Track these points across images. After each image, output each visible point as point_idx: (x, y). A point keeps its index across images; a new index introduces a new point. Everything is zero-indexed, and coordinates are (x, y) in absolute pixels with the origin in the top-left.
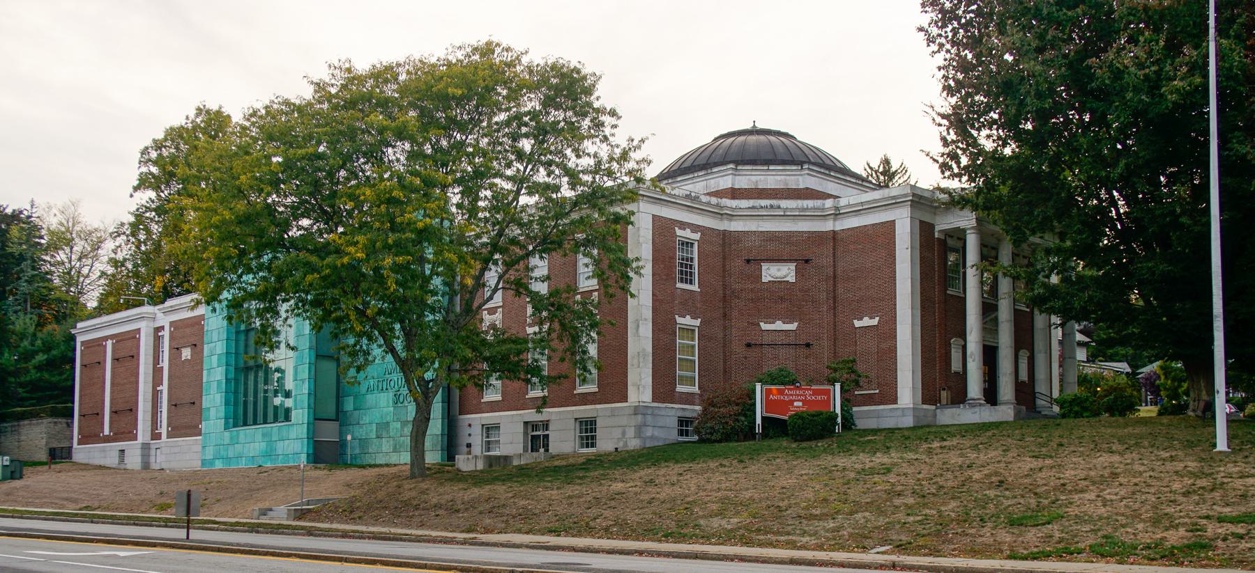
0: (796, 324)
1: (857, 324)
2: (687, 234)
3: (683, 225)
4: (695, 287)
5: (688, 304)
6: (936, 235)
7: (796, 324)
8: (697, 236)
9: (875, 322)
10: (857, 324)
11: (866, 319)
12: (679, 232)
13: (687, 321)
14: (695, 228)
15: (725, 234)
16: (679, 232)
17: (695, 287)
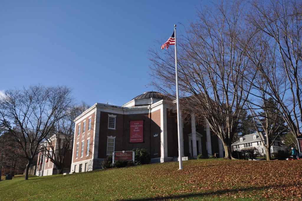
1: (155, 136)
3: (111, 114)
4: (114, 129)
5: (112, 133)
8: (115, 116)
12: (109, 115)
13: (111, 137)
14: (114, 114)
15: (124, 115)
16: (109, 115)
17: (114, 129)
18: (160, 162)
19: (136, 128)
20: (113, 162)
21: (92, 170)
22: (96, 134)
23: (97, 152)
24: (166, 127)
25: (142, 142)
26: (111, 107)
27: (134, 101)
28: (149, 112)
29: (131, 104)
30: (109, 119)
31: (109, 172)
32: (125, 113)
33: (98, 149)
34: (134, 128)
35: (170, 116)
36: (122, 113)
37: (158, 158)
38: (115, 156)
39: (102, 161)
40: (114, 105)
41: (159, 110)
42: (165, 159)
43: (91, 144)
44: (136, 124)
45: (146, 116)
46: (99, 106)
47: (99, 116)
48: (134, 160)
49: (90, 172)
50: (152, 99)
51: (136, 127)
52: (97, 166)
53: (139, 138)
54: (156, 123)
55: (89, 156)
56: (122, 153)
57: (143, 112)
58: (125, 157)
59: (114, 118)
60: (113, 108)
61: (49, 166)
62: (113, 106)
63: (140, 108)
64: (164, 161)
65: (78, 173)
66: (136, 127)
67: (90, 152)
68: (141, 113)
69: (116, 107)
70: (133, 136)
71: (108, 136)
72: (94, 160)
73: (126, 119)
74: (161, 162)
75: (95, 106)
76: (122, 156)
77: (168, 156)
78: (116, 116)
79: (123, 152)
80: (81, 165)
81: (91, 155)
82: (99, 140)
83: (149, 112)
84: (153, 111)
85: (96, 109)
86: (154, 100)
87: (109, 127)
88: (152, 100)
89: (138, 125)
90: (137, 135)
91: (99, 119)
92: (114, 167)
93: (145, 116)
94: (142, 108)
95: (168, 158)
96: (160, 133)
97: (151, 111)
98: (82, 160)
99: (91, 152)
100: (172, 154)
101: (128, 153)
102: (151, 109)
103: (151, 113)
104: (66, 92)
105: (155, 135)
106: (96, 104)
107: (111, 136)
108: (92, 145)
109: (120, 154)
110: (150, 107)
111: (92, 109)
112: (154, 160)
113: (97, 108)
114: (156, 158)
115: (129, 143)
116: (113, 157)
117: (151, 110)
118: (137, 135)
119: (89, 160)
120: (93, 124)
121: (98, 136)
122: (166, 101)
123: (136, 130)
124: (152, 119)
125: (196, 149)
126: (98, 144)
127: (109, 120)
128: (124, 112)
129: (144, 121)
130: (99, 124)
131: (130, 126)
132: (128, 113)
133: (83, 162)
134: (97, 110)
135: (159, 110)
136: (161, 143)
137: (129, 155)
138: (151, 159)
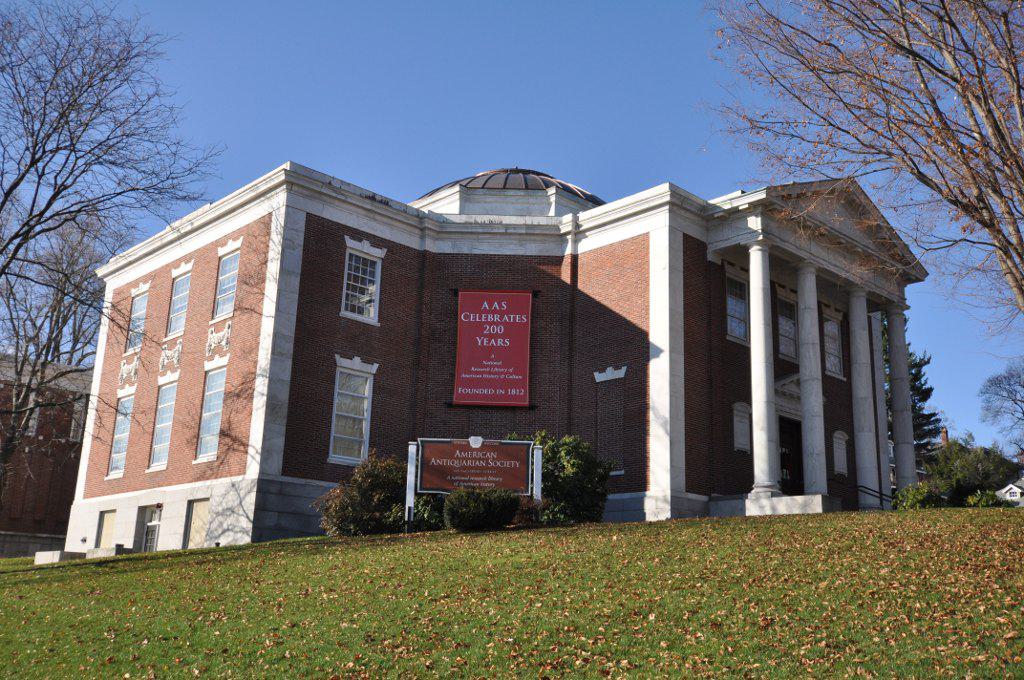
0: (624, 369)
1: (599, 377)
2: (365, 249)
3: (358, 235)
5: (359, 341)
6: (710, 257)
7: (624, 369)
8: (379, 253)
9: (621, 373)
10: (599, 377)
11: (610, 370)
12: (350, 242)
14: (377, 242)
15: (423, 255)
16: (350, 242)
18: (644, 515)
19: (488, 329)
20: (410, 500)
21: (246, 539)
22: (277, 336)
23: (280, 442)
24: (682, 330)
25: (521, 408)
26: (361, 196)
27: (457, 196)
28: (569, 251)
29: (447, 204)
30: (347, 267)
31: (375, 559)
32: (433, 246)
33: (285, 421)
34: (479, 328)
35: (707, 275)
36: (411, 241)
37: (634, 495)
38: (424, 466)
39: (312, 489)
40: (382, 192)
41: (644, 240)
42: (676, 504)
43: (239, 394)
44: (490, 305)
45: (549, 269)
46: (300, 182)
47: (300, 239)
48: (537, 493)
49: (235, 551)
50: (556, 193)
51: (492, 323)
52: (279, 518)
53: (507, 384)
54: (617, 310)
55: (221, 460)
56: (467, 448)
57: (532, 249)
58: (482, 471)
59: (373, 264)
60: (381, 209)
61: (845, 379)
62: (372, 198)
63: (515, 226)
64: (673, 510)
65: (659, 524)
66: (492, 323)
67: (232, 439)
68: (520, 251)
69: (386, 203)
70: (475, 372)
71: (344, 356)
72: (263, 486)
73: (436, 282)
74: (650, 518)
75: (283, 177)
76: (464, 468)
77: (689, 489)
78: (386, 250)
79: (476, 442)
80: (145, 513)
81: (233, 458)
82: (294, 371)
83: (569, 251)
84: (585, 246)
85: (280, 198)
86: (565, 201)
87: (346, 309)
88: (553, 199)
89: (502, 314)
90: (494, 368)
91: (299, 253)
92: (418, 525)
93: (544, 272)
94: (527, 226)
95: (691, 496)
96: (648, 360)
97: (575, 247)
98: (159, 480)
99: (235, 440)
100: (715, 472)
101: (505, 452)
102: (579, 233)
103: (575, 258)
104: (120, 62)
105: (602, 370)
106: (287, 166)
107: (357, 360)
108: (251, 397)
109: (451, 456)
110: (577, 225)
111: (253, 194)
112: (623, 500)
113: (289, 191)
114: (627, 496)
115: (450, 405)
116: (411, 470)
117: (576, 242)
118: (494, 368)
119: (226, 481)
120: (252, 280)
121: (289, 347)
122: (557, 233)
123: (490, 336)
124: (580, 286)
125: (823, 459)
126: (284, 396)
127: (346, 271)
128: (422, 238)
129: (535, 294)
130: (296, 282)
131: (456, 315)
132: (444, 247)
133: (173, 497)
134: (288, 199)
135: (644, 240)
136: (652, 416)
137: (507, 464)
138: (611, 497)
